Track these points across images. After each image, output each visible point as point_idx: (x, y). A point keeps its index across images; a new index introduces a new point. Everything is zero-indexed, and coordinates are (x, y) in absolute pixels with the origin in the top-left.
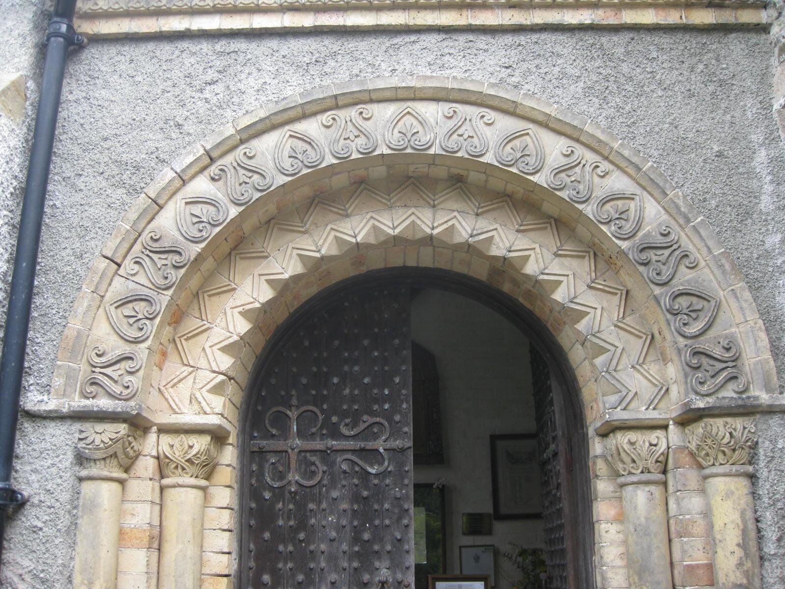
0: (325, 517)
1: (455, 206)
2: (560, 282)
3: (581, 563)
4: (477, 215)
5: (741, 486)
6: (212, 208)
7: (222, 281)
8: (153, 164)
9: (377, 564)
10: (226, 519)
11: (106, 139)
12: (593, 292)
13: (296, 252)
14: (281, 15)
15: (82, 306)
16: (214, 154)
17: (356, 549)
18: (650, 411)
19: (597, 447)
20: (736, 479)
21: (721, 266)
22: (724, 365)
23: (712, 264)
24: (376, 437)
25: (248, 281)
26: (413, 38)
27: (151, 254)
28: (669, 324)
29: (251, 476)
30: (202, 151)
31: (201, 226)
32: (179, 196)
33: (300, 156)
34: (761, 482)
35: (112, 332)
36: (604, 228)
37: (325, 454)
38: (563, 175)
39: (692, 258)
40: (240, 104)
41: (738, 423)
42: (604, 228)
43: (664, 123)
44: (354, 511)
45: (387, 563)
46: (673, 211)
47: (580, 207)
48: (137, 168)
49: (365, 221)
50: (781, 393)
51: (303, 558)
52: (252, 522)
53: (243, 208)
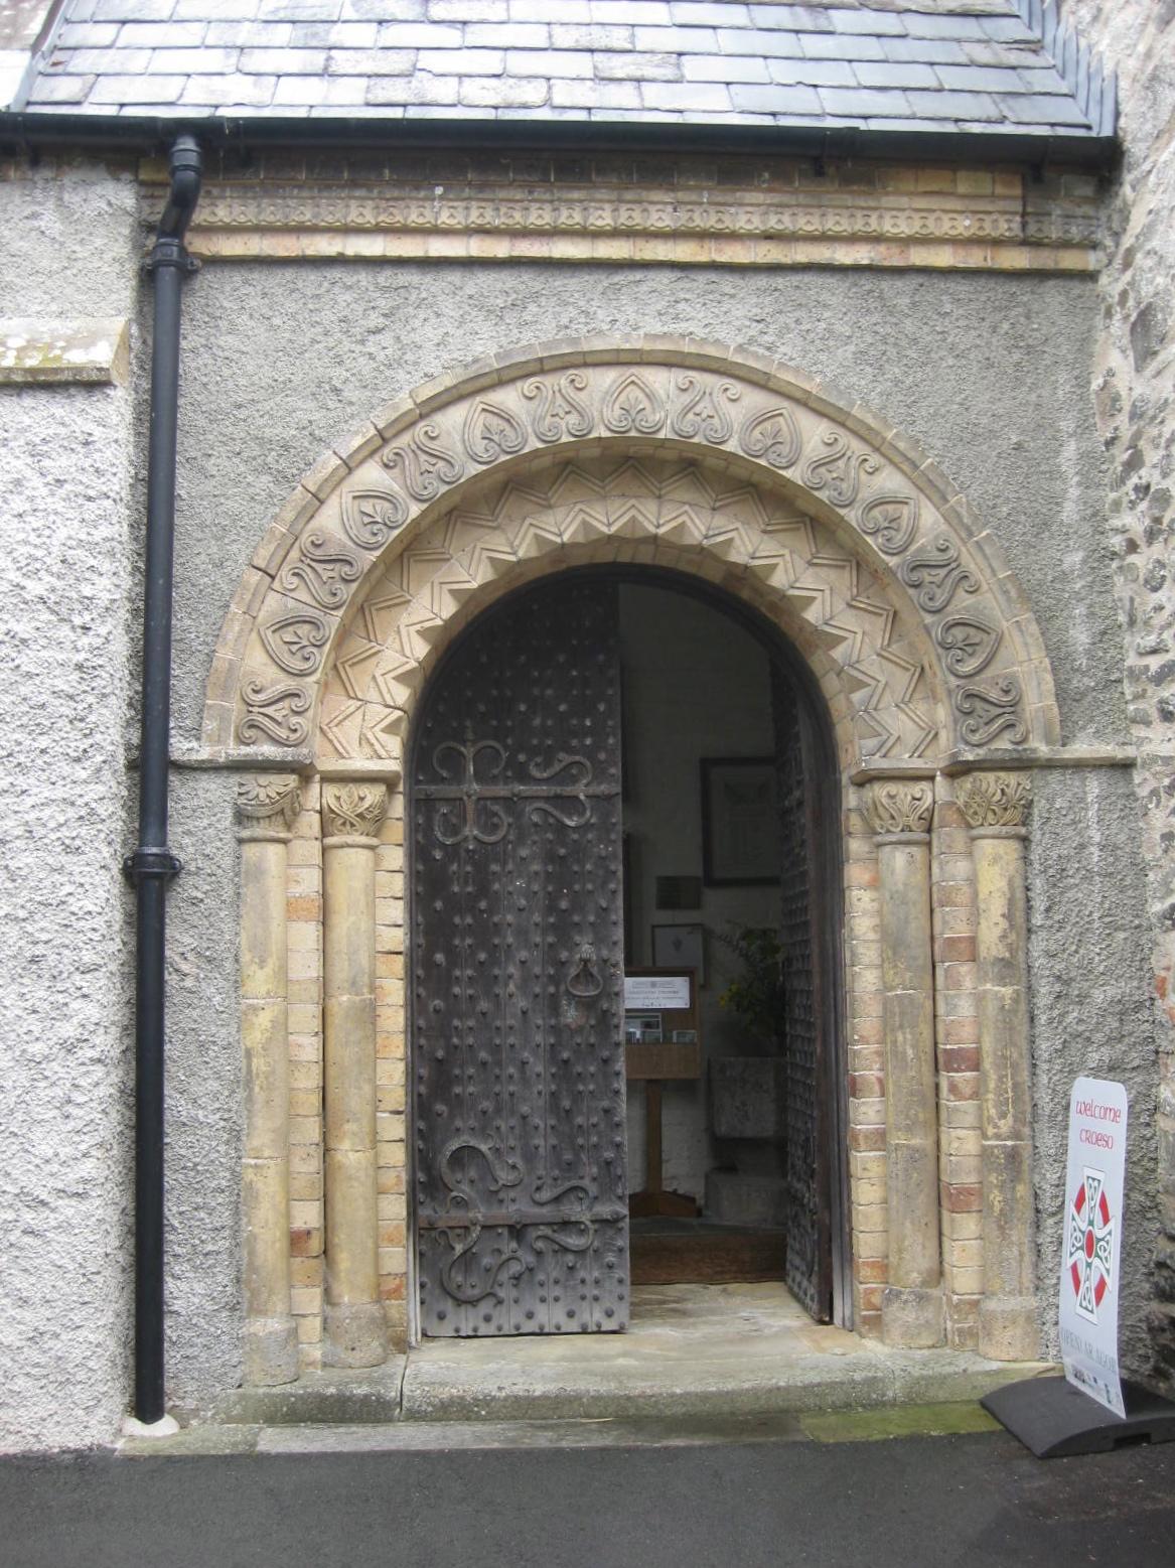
0: (512, 882)
1: (687, 497)
2: (813, 599)
3: (828, 937)
4: (714, 509)
5: (1010, 850)
6: (387, 505)
7: (393, 588)
8: (306, 444)
9: (577, 939)
10: (398, 884)
11: (239, 407)
12: (854, 612)
13: (486, 554)
14: (465, 239)
15: (233, 630)
16: (387, 435)
17: (552, 920)
18: (914, 759)
19: (851, 798)
20: (1005, 842)
21: (1006, 592)
22: (1001, 710)
23: (995, 588)
24: (574, 780)
25: (426, 591)
26: (638, 275)
27: (313, 564)
28: (939, 660)
29: (417, 831)
30: (373, 432)
31: (375, 528)
32: (345, 487)
33: (496, 438)
34: (1033, 846)
35: (269, 661)
36: (869, 539)
37: (509, 802)
38: (822, 470)
39: (972, 580)
40: (416, 363)
41: (1012, 778)
42: (869, 539)
43: (953, 402)
44: (547, 873)
45: (590, 937)
46: (955, 522)
47: (842, 512)
48: (286, 448)
49: (572, 514)
50: (1064, 745)
51: (485, 932)
52: (420, 889)
53: (425, 505)
